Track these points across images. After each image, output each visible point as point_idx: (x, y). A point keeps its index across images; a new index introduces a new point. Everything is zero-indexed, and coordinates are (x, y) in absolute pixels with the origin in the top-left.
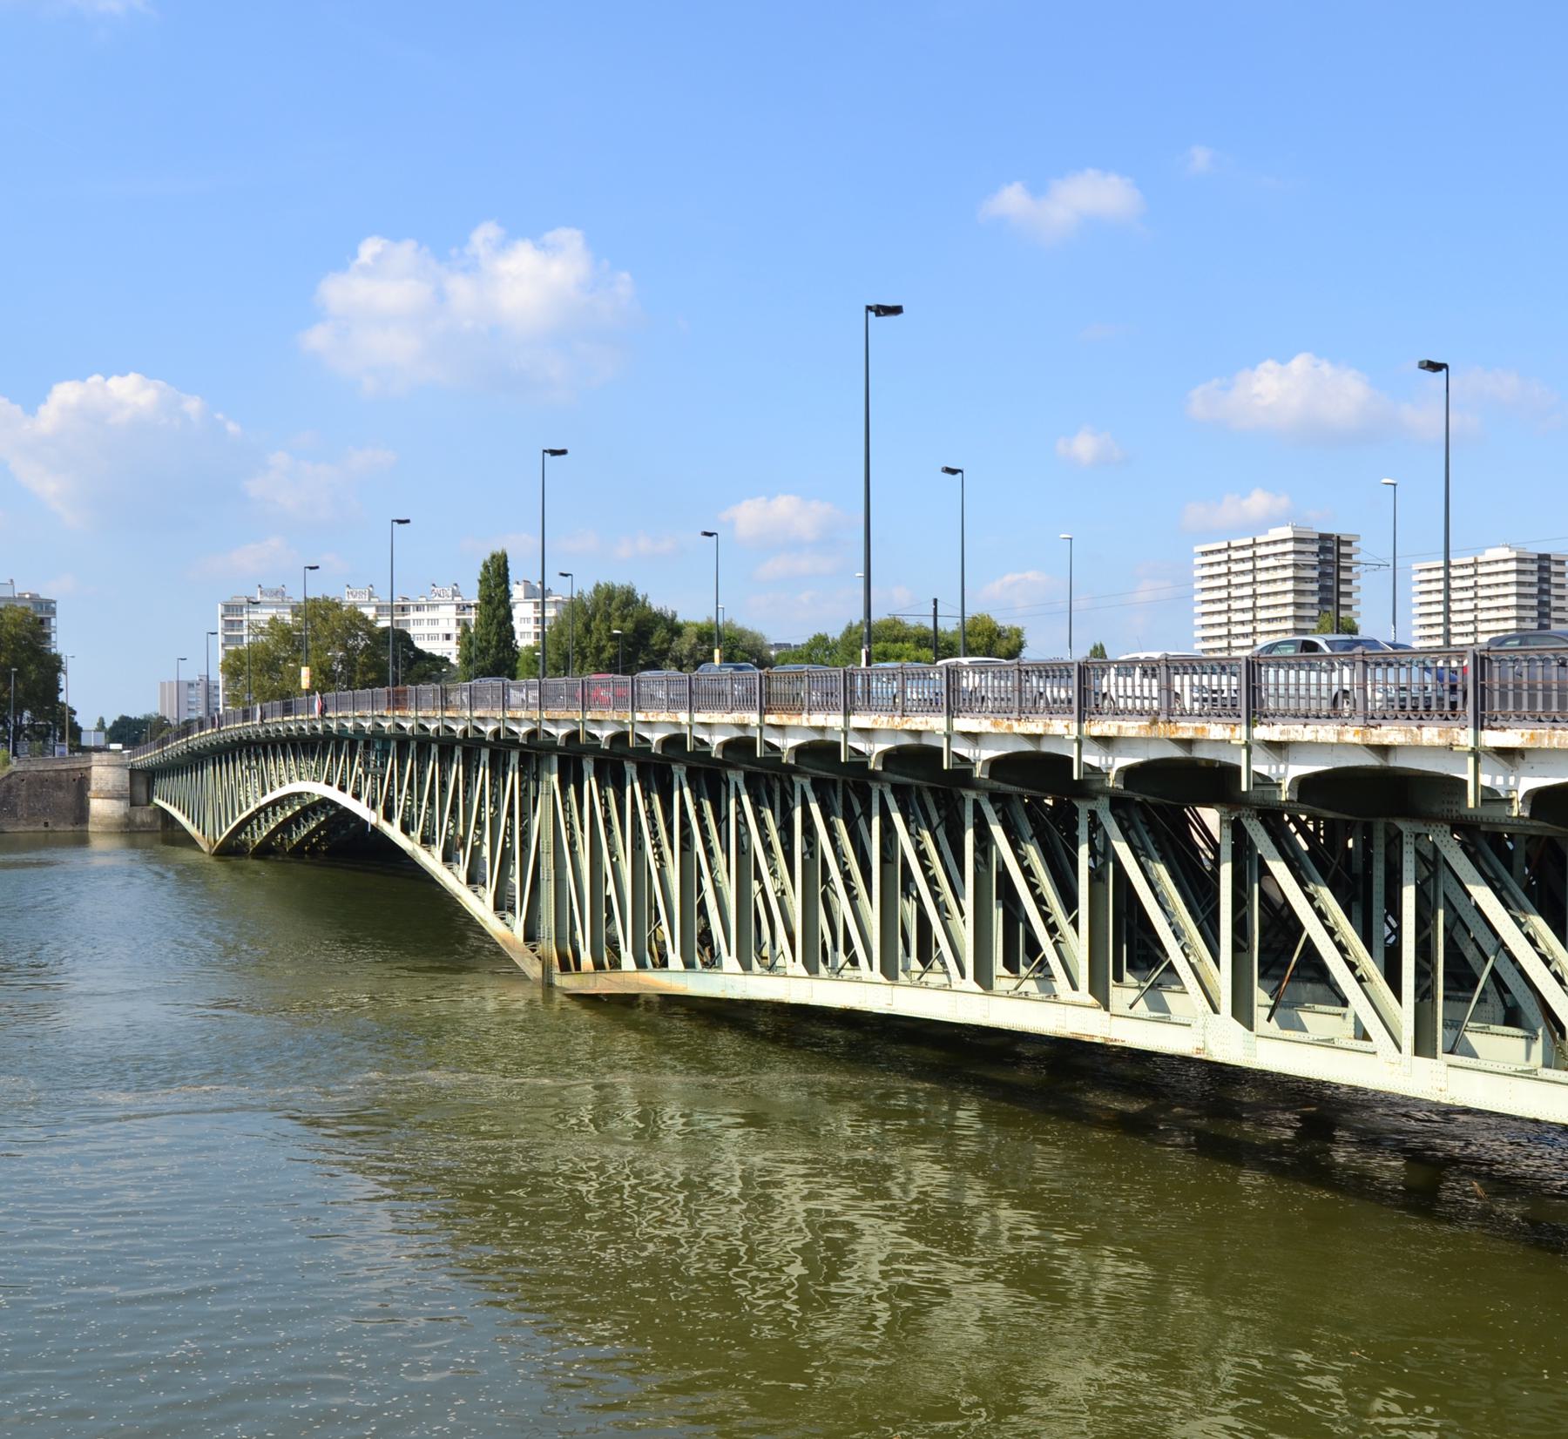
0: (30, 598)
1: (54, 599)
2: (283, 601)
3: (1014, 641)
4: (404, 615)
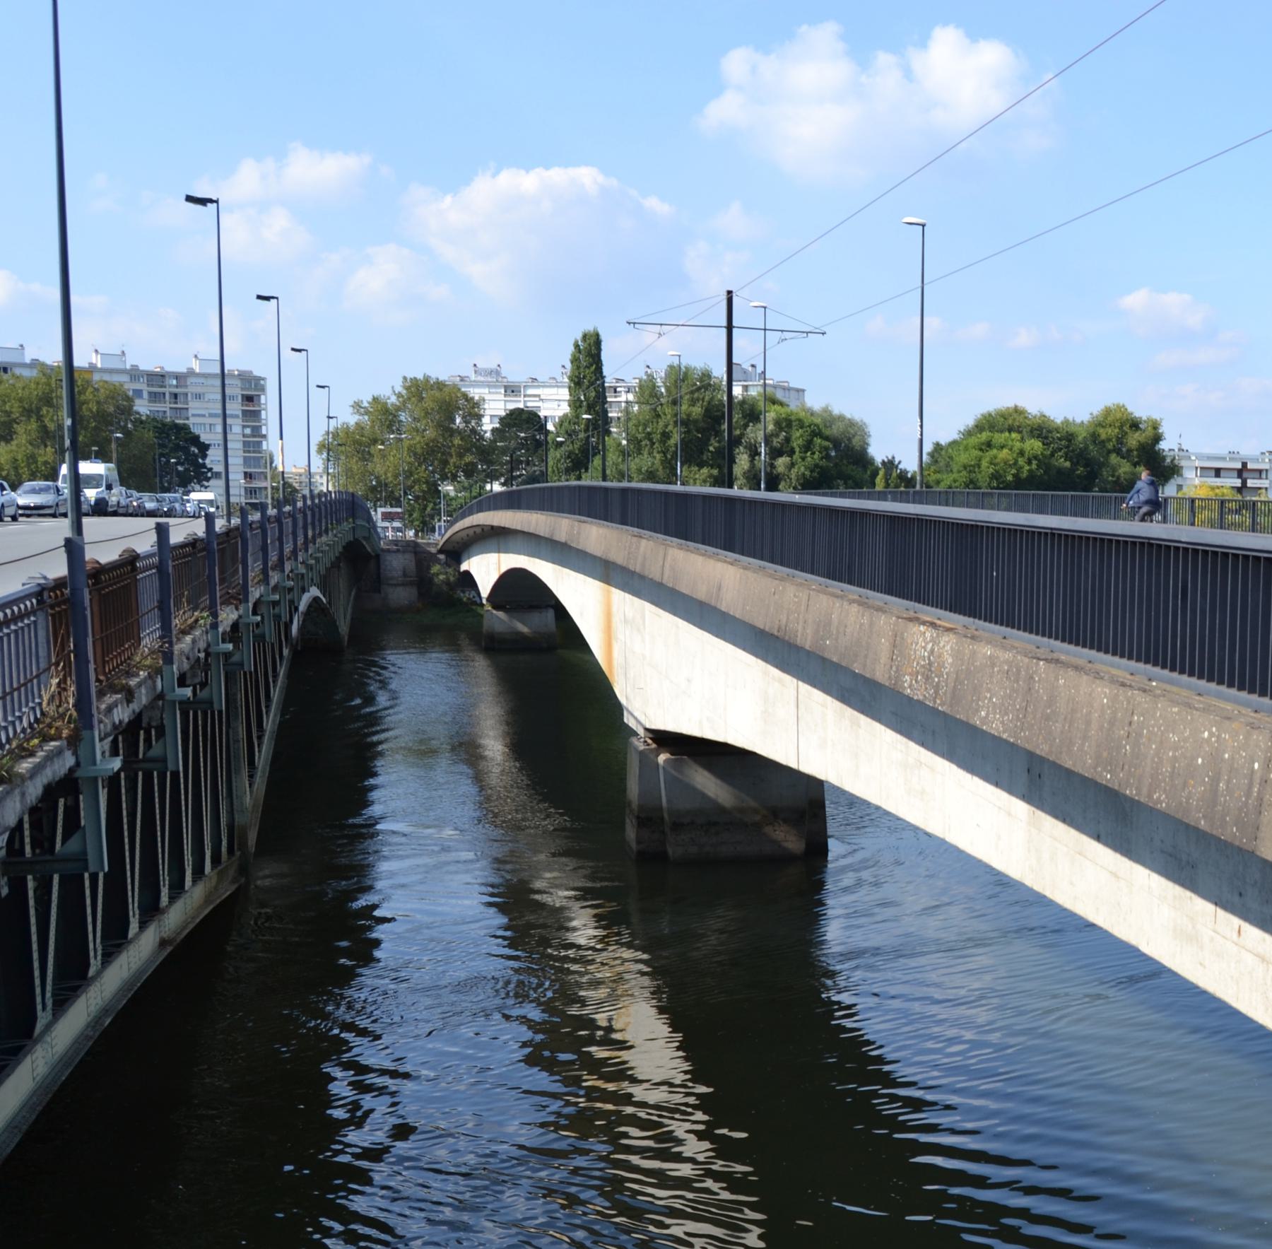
0: (239, 375)
1: (263, 376)
2: (497, 381)
3: (1150, 432)
4: (616, 397)
